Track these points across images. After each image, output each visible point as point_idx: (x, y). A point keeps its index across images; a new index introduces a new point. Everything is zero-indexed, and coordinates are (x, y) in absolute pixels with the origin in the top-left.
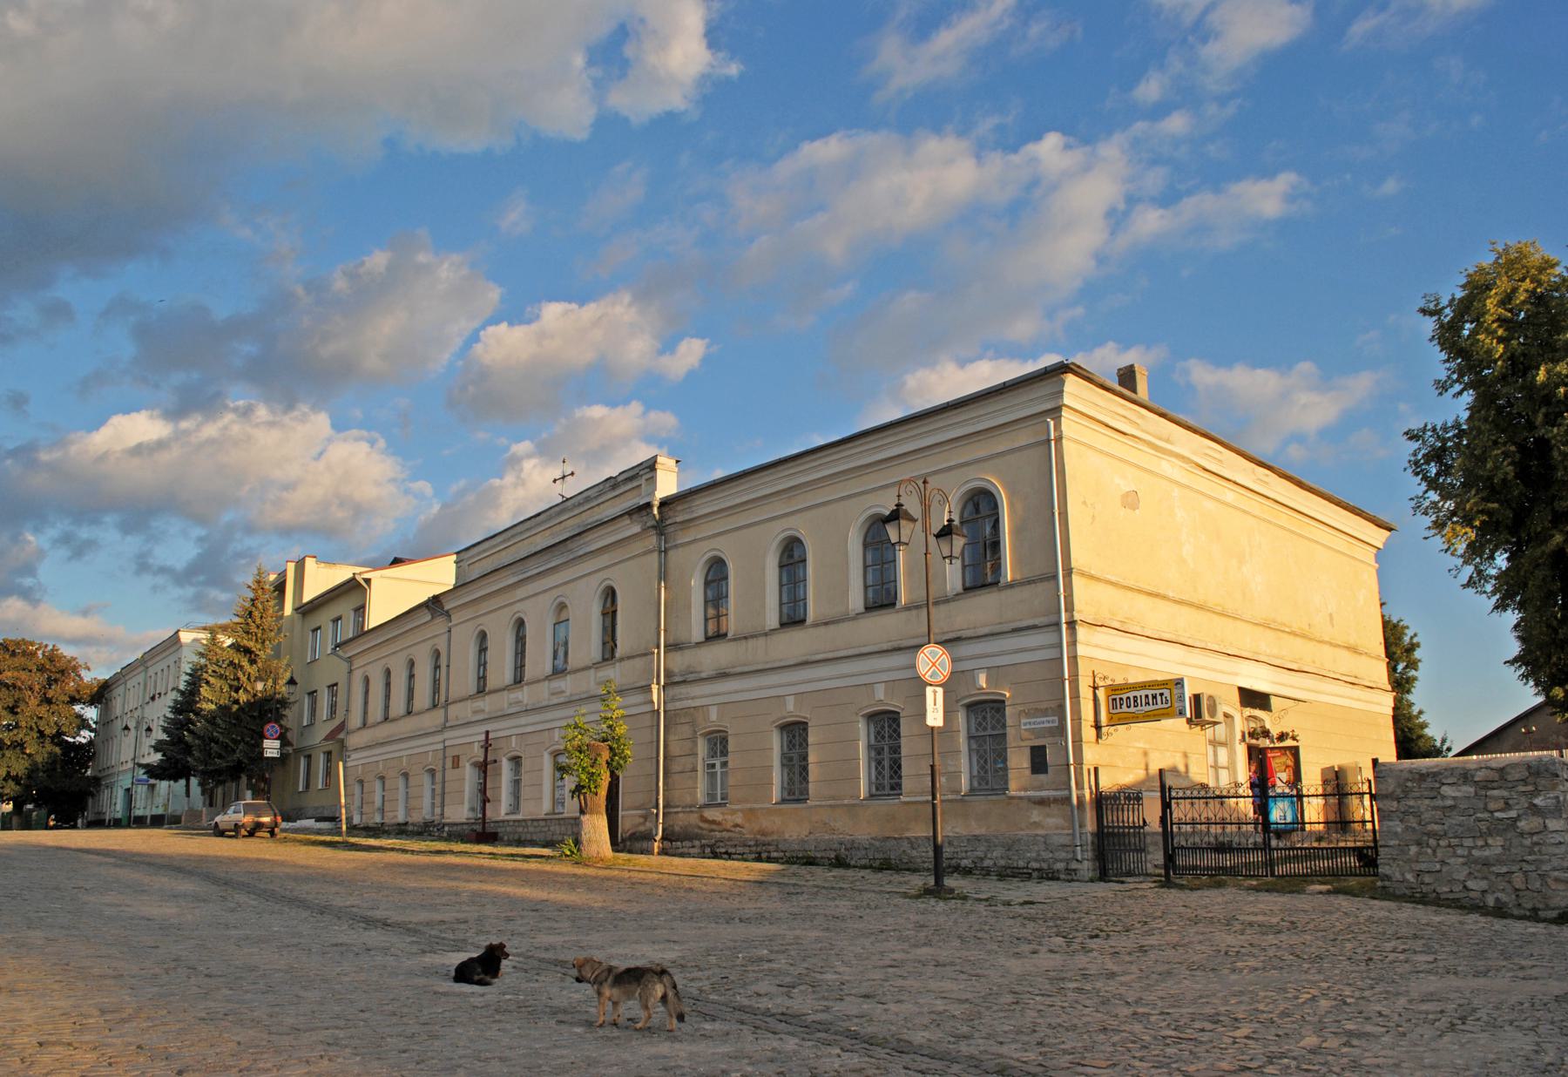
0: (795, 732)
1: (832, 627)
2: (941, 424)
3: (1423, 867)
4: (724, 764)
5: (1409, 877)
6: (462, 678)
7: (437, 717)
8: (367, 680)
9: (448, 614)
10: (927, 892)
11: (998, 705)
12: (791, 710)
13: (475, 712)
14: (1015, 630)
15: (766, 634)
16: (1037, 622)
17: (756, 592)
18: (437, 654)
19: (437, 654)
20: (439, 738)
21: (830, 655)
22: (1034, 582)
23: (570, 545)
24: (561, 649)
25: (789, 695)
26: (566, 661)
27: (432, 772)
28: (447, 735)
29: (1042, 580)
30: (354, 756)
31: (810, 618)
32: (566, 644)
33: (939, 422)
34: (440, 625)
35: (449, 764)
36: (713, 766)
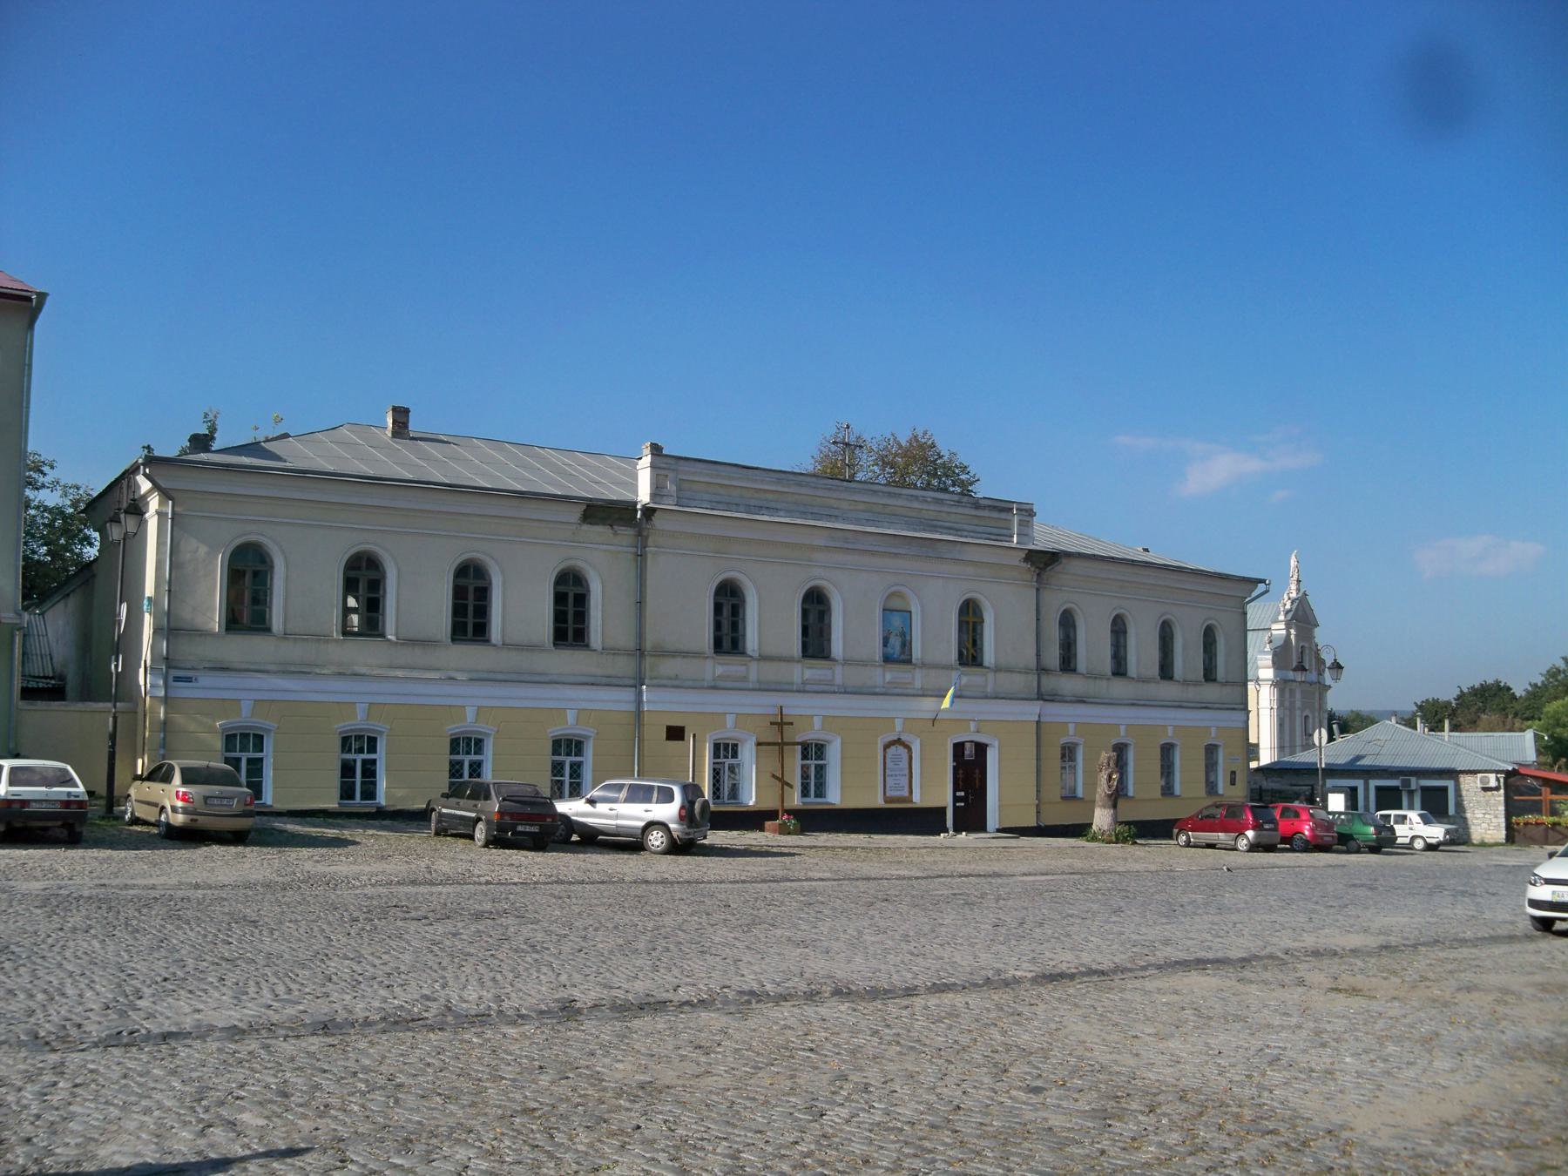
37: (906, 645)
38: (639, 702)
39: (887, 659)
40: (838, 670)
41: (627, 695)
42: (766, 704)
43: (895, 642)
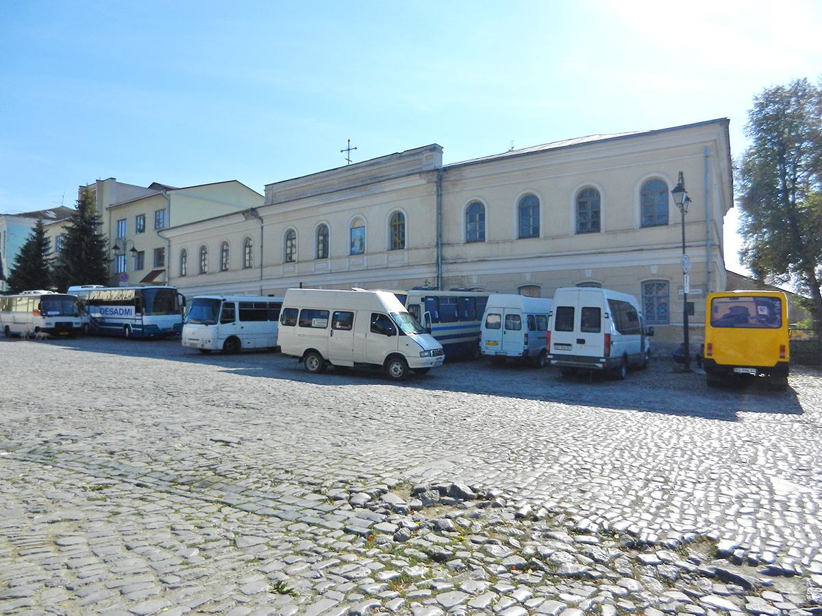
12: (654, 273)
28: (263, 283)
37: (362, 245)
39: (352, 253)
40: (329, 262)
43: (357, 244)
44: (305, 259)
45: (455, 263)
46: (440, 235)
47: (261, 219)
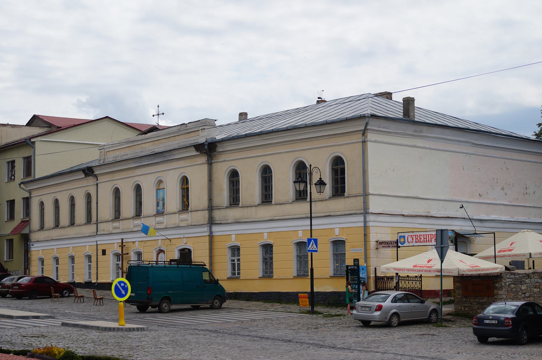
0: (268, 248)
1: (282, 206)
2: (324, 129)
3: (467, 305)
4: (239, 260)
5: (463, 308)
6: (105, 208)
7: (91, 229)
8: (42, 204)
9: (96, 176)
10: (309, 312)
11: (342, 242)
13: (115, 228)
14: (325, 216)
15: (256, 206)
16: (357, 212)
17: (251, 186)
18: (89, 196)
19: (89, 196)
20: (94, 239)
21: (75, 236)
22: (322, 200)
23: (165, 154)
24: (160, 203)
25: (265, 232)
26: (163, 208)
27: (89, 257)
28: (98, 238)
29: (359, 196)
30: (36, 245)
31: (273, 202)
32: (163, 200)
33: (324, 128)
34: (91, 181)
35: (100, 252)
36: (234, 261)
38: (211, 232)
40: (142, 219)
41: (361, 218)
42: (117, 240)
44: (248, 204)
45: (221, 224)
46: (210, 200)
47: (96, 176)
